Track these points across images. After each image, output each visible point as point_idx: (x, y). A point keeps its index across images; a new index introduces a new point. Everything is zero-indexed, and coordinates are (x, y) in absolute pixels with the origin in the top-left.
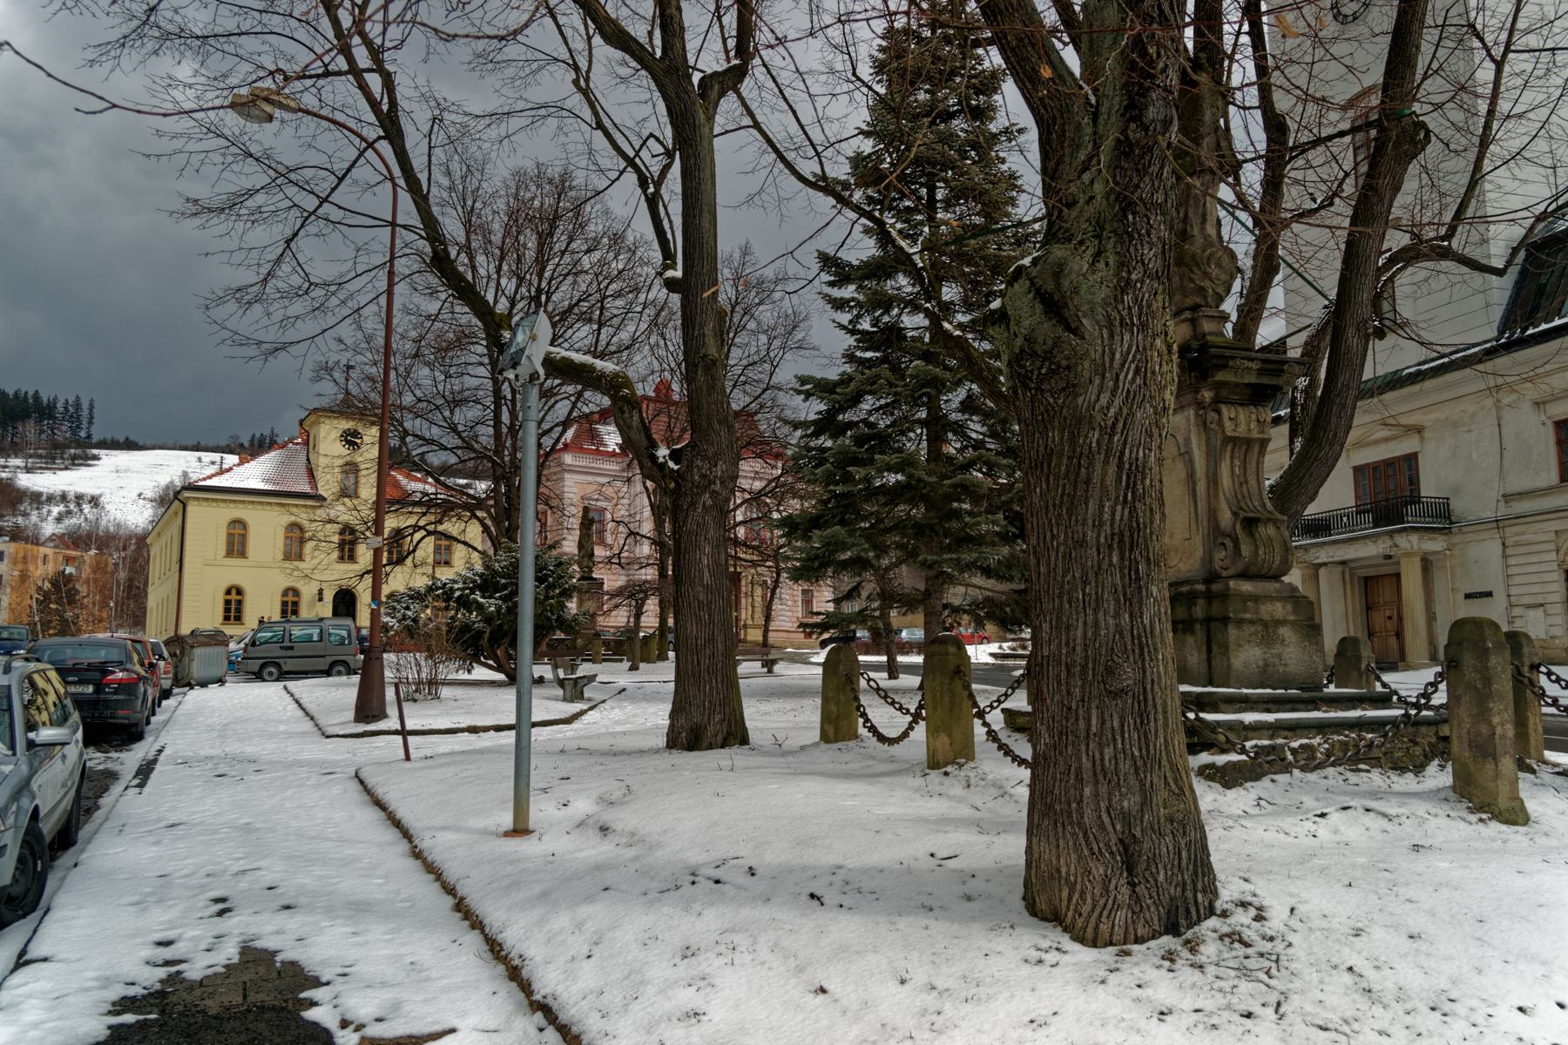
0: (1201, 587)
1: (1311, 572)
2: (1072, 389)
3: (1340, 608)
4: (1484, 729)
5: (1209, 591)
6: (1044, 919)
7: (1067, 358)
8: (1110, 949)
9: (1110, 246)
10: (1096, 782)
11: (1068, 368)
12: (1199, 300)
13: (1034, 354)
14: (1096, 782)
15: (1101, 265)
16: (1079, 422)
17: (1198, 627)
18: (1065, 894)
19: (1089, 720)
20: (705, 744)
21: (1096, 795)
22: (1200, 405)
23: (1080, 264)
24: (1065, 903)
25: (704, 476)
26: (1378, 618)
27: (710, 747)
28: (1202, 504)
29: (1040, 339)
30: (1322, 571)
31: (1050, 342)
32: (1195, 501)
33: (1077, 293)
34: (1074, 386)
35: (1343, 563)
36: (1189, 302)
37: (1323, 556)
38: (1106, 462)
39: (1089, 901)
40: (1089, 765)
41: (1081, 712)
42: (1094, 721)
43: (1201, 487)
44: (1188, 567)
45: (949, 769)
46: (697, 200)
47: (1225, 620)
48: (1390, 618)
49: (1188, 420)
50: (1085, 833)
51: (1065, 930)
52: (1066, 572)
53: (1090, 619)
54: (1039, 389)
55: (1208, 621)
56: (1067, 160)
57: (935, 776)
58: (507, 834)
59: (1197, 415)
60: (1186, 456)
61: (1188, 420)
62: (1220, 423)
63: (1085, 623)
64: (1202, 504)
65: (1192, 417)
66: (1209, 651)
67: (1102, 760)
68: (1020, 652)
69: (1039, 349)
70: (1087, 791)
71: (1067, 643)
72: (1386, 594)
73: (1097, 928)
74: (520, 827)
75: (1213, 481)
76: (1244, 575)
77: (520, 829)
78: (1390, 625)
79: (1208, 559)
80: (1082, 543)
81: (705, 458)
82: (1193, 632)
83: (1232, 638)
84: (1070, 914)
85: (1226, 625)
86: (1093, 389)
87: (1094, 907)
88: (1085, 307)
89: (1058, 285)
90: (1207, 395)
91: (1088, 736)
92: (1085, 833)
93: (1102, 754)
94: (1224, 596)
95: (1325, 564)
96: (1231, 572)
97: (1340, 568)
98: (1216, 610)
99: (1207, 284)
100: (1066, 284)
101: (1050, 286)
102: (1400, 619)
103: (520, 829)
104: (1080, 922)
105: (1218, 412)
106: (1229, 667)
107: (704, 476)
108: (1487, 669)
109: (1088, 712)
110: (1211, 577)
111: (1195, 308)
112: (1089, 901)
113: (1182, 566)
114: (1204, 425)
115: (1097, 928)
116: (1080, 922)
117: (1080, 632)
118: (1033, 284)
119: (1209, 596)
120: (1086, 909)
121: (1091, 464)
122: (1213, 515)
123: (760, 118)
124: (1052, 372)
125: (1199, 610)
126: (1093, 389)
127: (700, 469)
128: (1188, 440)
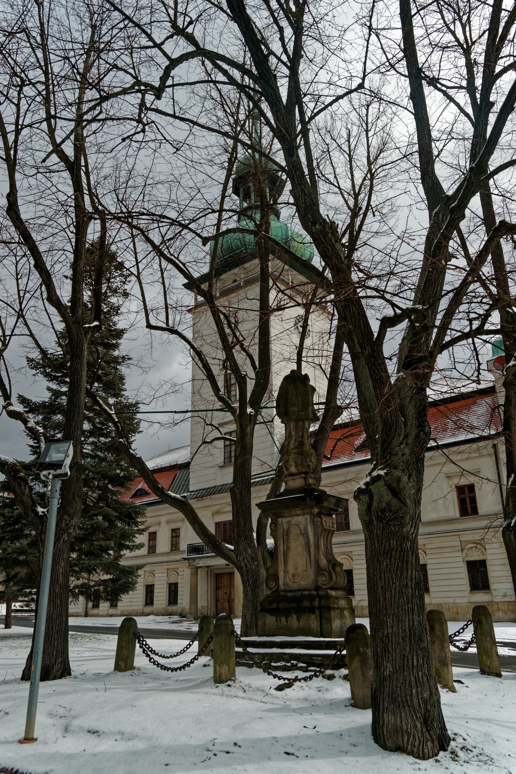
0: (314, 593)
1: (195, 570)
2: (403, 525)
3: (205, 588)
4: (443, 655)
5: (318, 594)
6: (391, 751)
7: (403, 514)
8: (431, 760)
9: (414, 473)
10: (417, 687)
11: (402, 517)
12: (308, 470)
13: (390, 510)
14: (417, 687)
15: (412, 480)
16: (404, 539)
17: (317, 611)
18: (406, 738)
19: (413, 660)
20: (52, 676)
21: (417, 692)
22: (311, 514)
23: (405, 479)
24: (405, 742)
25: (67, 525)
26: (221, 593)
27: (55, 678)
28: (312, 556)
29: (394, 505)
30: (199, 570)
31: (398, 507)
32: (310, 555)
33: (404, 489)
34: (403, 524)
35: (208, 567)
36: (304, 470)
37: (201, 563)
38: (412, 555)
39: (417, 740)
40: (414, 680)
41: (410, 657)
42: (415, 661)
43: (312, 549)
44: (305, 583)
45: (229, 683)
46: (80, 385)
47: (329, 608)
48: (226, 593)
49: (306, 519)
50: (414, 709)
51: (408, 754)
52: (400, 598)
53: (411, 618)
54: (387, 523)
55: (320, 608)
56: (395, 439)
57: (222, 687)
58: (20, 742)
59: (311, 518)
60: (305, 535)
61: (306, 519)
62: (321, 523)
63: (409, 620)
64: (312, 556)
65: (308, 519)
66: (321, 621)
67: (418, 677)
68: (25, 608)
69: (393, 509)
70: (414, 691)
71: (402, 628)
72: (225, 582)
73: (423, 751)
74: (30, 736)
75: (317, 547)
76: (332, 588)
77: (28, 738)
78: (226, 597)
79: (316, 580)
80: (406, 586)
81: (69, 515)
82: (314, 613)
83: (332, 616)
84: (409, 747)
85: (330, 610)
86: (409, 526)
87: (420, 742)
88: (407, 495)
89: (399, 485)
90: (316, 510)
91: (413, 667)
92: (414, 709)
93: (418, 675)
94: (328, 597)
95: (201, 567)
96: (328, 586)
97: (206, 569)
98: (324, 602)
99: (311, 464)
100: (402, 485)
101: (395, 485)
102: (230, 594)
103: (28, 738)
104: (415, 750)
105: (321, 518)
106: (331, 628)
107: (67, 525)
108: (443, 630)
109: (413, 657)
110: (317, 588)
111: (306, 473)
112: (417, 740)
113: (302, 582)
114: (314, 523)
115: (423, 751)
116: (415, 750)
117: (407, 623)
118: (385, 483)
119: (320, 597)
120: (417, 743)
121: (408, 555)
122: (317, 562)
123: (34, 332)
124: (396, 518)
125: (316, 603)
126: (409, 526)
127: (66, 520)
128: (306, 528)
